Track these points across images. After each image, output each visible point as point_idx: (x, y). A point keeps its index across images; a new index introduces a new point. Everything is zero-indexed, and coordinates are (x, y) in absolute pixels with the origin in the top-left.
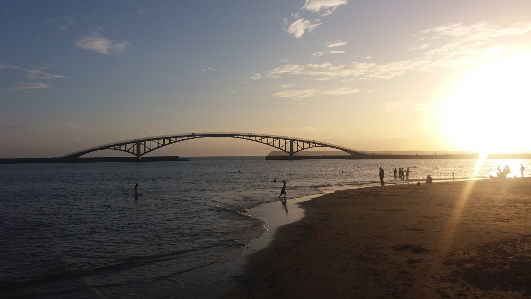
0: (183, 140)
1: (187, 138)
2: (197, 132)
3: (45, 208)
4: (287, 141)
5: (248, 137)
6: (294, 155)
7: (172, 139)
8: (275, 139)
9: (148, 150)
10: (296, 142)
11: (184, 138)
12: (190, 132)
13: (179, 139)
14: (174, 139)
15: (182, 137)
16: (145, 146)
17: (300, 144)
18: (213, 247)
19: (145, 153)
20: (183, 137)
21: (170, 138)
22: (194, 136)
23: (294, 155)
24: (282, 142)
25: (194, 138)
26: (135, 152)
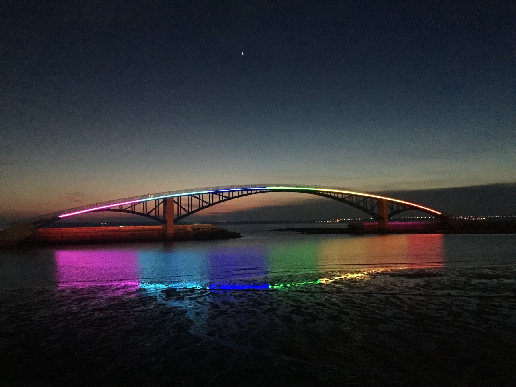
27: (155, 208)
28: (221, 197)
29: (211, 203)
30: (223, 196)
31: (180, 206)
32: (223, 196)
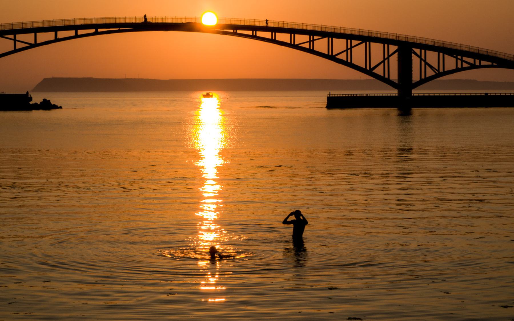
0: (77, 36)
1: (72, 33)
2: (156, 15)
3: (306, 195)
4: (393, 48)
5: (267, 35)
6: (415, 92)
7: (19, 37)
8: (355, 42)
9: (430, 73)
10: (417, 51)
11: (61, 34)
12: (135, 15)
13: (42, 37)
14: (29, 38)
15: (55, 29)
16: (424, 60)
17: (432, 57)
18: (28, 318)
19: (423, 81)
20: (78, 29)
21: (15, 32)
22: (146, 26)
23: (415, 92)
24: (377, 49)
25: (97, 33)
26: (394, 76)
27: (383, 62)
28: (459, 62)
29: (441, 70)
30: (462, 61)
31: (421, 59)
32: (462, 61)
